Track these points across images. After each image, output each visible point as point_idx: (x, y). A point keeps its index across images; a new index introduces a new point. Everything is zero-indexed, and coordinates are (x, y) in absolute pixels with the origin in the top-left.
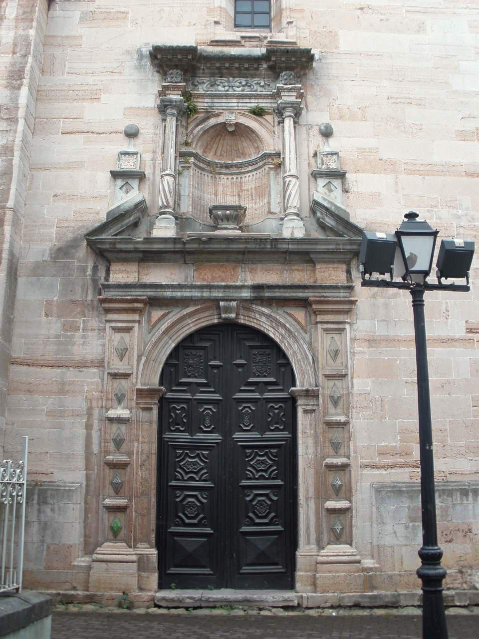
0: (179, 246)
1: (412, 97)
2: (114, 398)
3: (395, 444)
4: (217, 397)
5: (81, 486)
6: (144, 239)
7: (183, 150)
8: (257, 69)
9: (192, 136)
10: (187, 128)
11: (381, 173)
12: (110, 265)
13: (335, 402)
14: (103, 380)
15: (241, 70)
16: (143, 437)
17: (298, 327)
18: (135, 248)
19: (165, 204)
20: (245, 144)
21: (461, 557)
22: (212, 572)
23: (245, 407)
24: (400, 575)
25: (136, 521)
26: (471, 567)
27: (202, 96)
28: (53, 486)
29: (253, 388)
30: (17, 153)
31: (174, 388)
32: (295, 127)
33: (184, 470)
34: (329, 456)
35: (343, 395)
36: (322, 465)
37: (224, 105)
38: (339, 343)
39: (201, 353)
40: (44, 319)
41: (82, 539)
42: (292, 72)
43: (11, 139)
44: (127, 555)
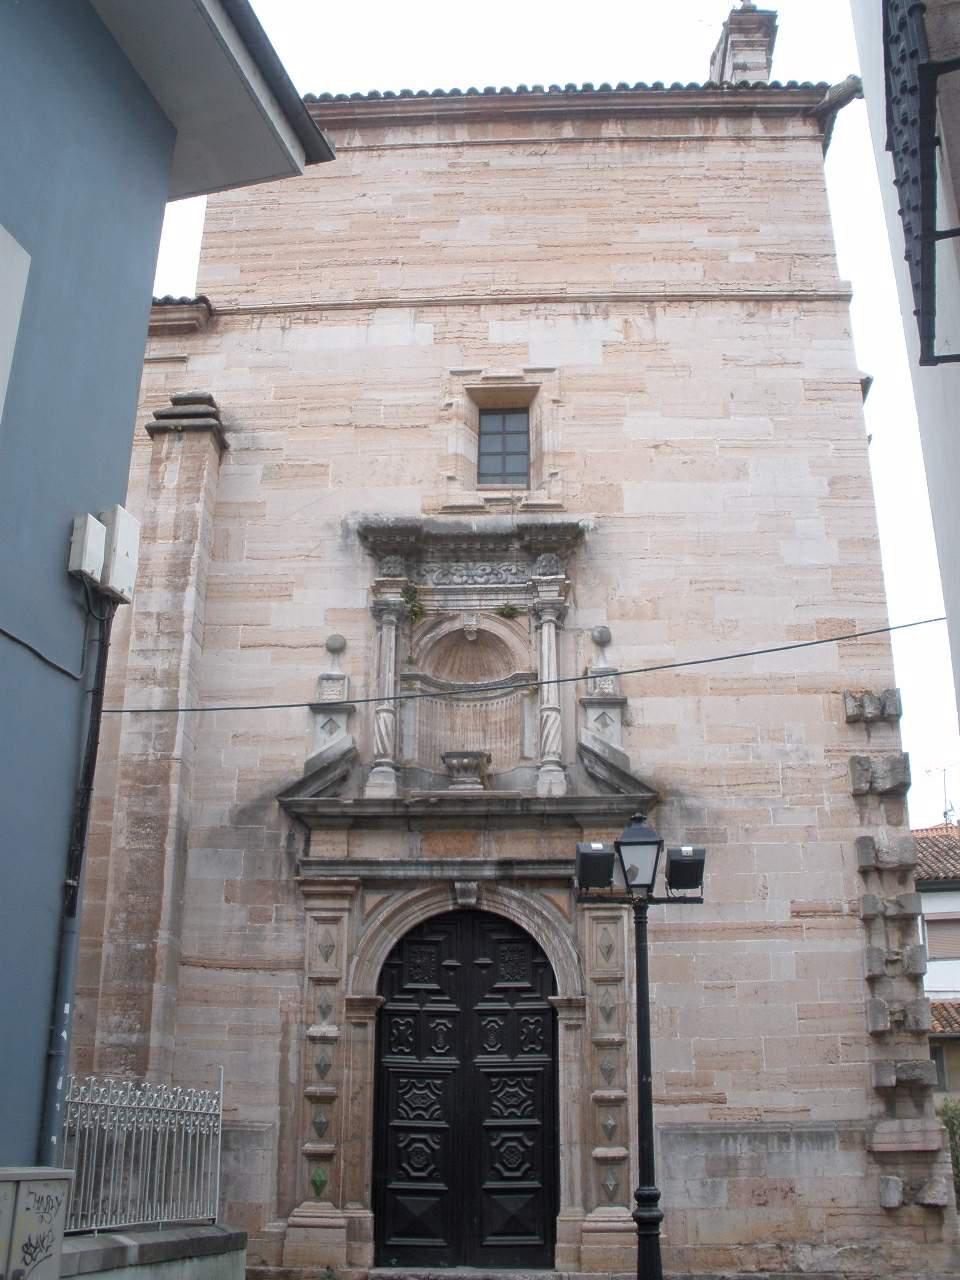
0: (400, 810)
1: (725, 578)
2: (317, 1009)
4: (453, 1008)
5: (274, 1125)
6: (355, 800)
7: (406, 672)
8: (507, 550)
9: (418, 650)
10: (411, 637)
12: (310, 834)
13: (608, 1015)
14: (302, 987)
15: (485, 551)
16: (355, 1062)
17: (560, 915)
18: (342, 812)
19: (382, 751)
20: (492, 658)
22: (445, 1244)
23: (438, 1024)
24: (695, 1250)
25: (345, 1173)
27: (432, 592)
28: (237, 1126)
29: (500, 996)
30: (183, 683)
31: (397, 997)
32: (557, 635)
33: (409, 1105)
34: (599, 1088)
35: (618, 1005)
36: (589, 1097)
37: (461, 603)
38: (613, 936)
39: (432, 949)
40: (224, 905)
41: (275, 1198)
42: (554, 555)
43: (174, 661)
44: (332, 1218)
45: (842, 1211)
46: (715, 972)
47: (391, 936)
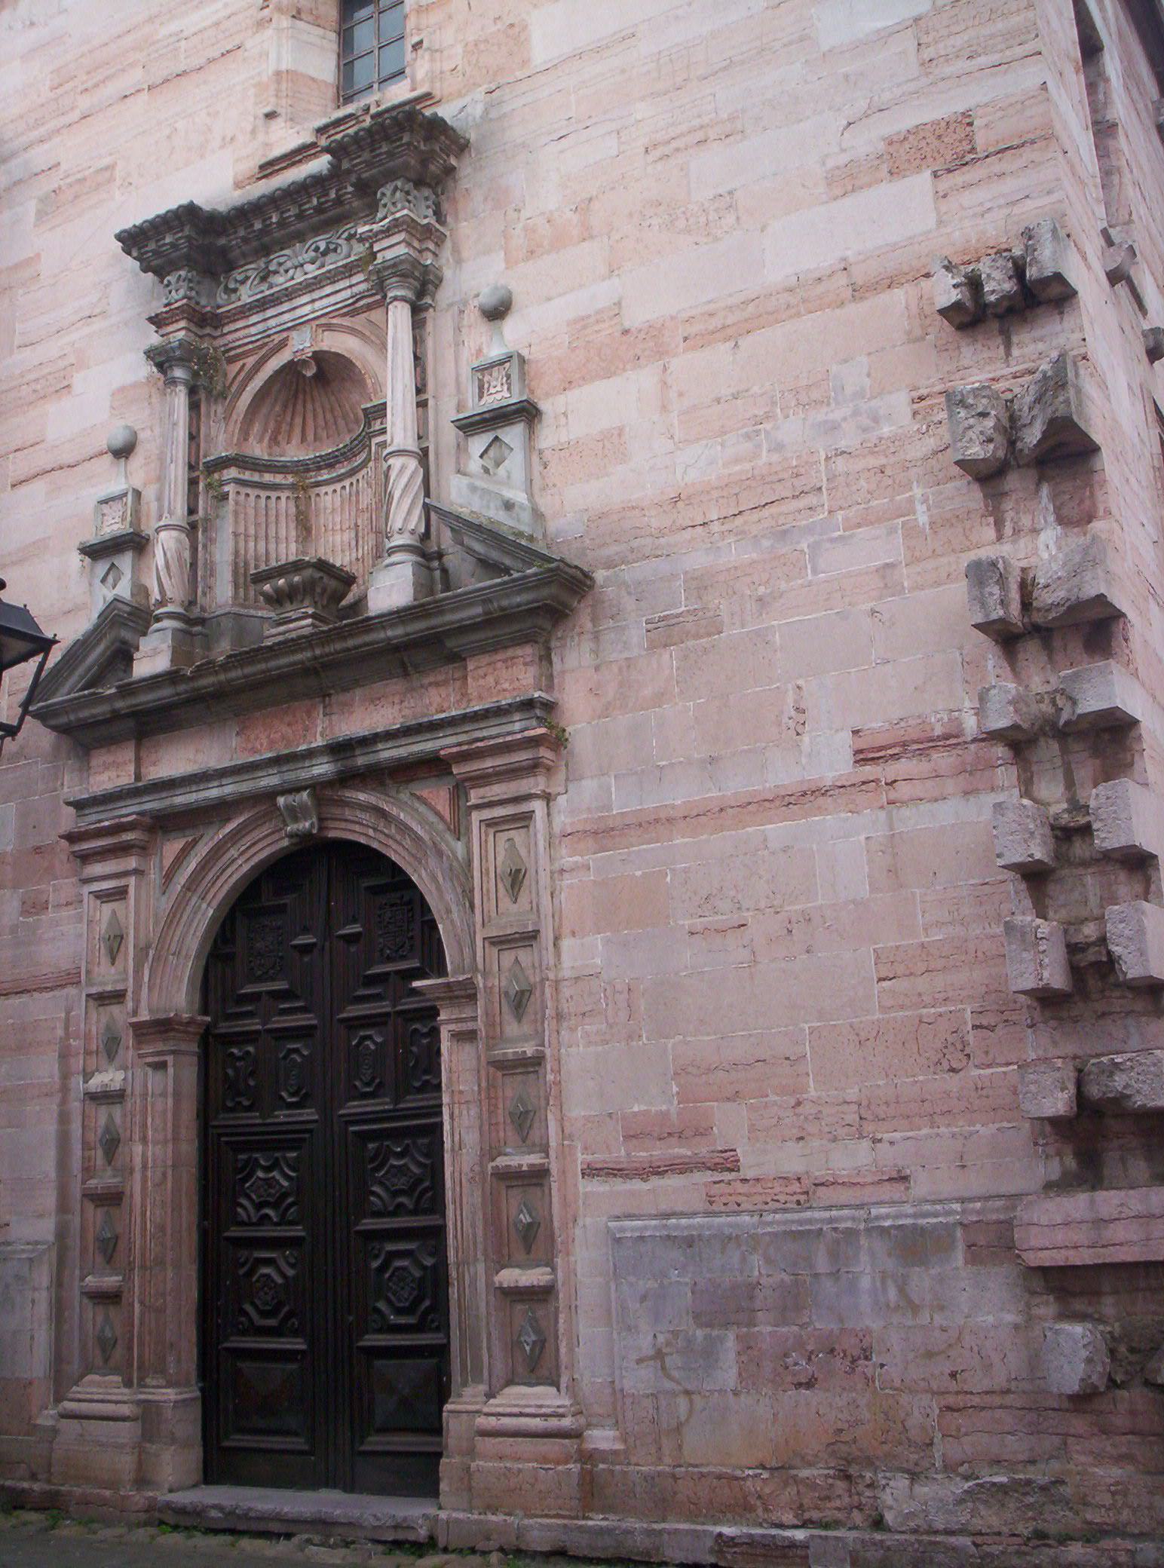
3: (664, 1108)
11: (624, 370)
21: (841, 1431)
22: (306, 1447)
26: (870, 1462)
37: (287, 317)
45: (976, 1400)
47: (204, 906)
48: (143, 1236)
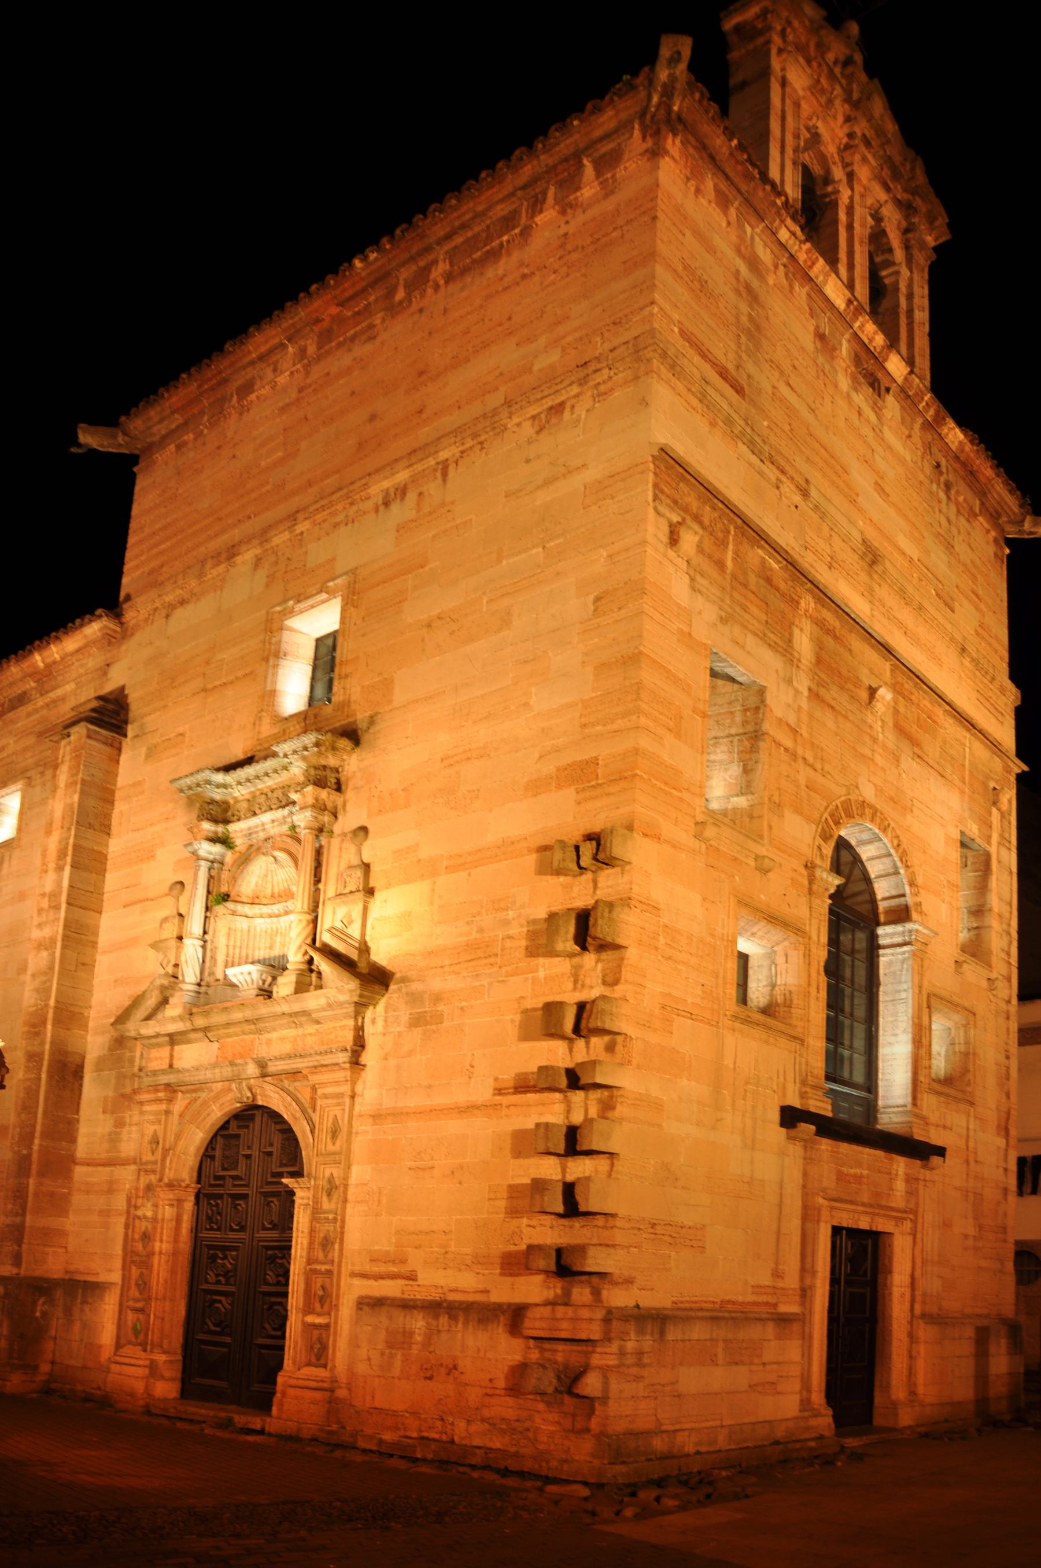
40: (101, 1116)
46: (419, 1153)
48: (157, 1284)
